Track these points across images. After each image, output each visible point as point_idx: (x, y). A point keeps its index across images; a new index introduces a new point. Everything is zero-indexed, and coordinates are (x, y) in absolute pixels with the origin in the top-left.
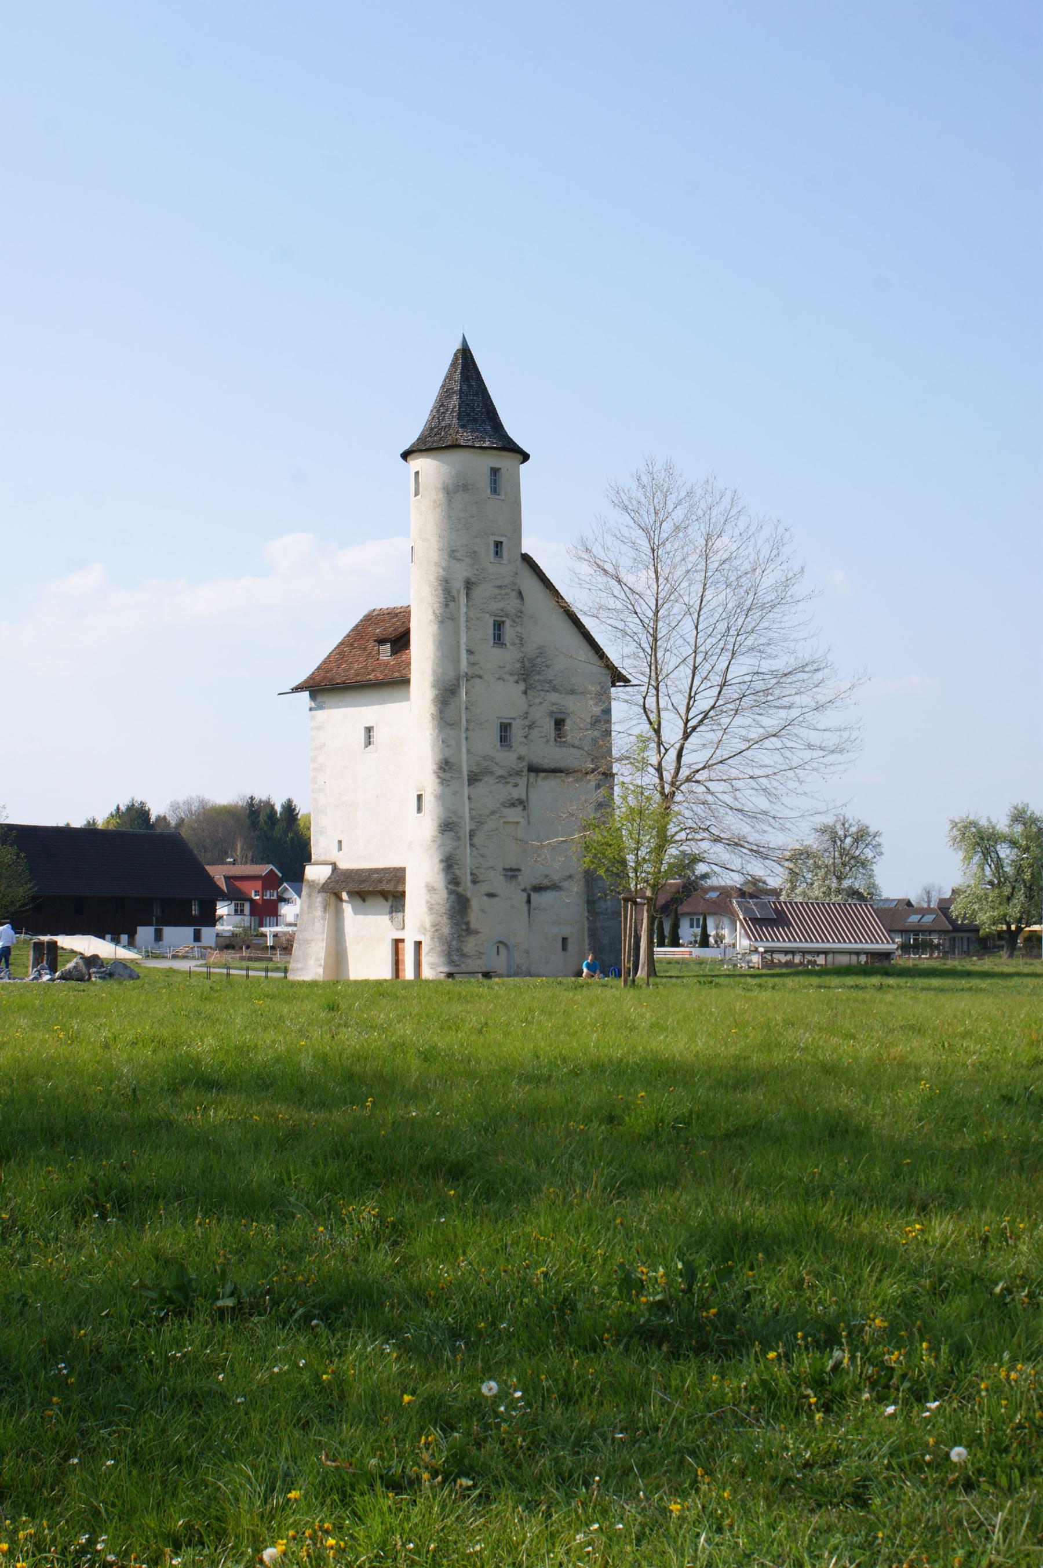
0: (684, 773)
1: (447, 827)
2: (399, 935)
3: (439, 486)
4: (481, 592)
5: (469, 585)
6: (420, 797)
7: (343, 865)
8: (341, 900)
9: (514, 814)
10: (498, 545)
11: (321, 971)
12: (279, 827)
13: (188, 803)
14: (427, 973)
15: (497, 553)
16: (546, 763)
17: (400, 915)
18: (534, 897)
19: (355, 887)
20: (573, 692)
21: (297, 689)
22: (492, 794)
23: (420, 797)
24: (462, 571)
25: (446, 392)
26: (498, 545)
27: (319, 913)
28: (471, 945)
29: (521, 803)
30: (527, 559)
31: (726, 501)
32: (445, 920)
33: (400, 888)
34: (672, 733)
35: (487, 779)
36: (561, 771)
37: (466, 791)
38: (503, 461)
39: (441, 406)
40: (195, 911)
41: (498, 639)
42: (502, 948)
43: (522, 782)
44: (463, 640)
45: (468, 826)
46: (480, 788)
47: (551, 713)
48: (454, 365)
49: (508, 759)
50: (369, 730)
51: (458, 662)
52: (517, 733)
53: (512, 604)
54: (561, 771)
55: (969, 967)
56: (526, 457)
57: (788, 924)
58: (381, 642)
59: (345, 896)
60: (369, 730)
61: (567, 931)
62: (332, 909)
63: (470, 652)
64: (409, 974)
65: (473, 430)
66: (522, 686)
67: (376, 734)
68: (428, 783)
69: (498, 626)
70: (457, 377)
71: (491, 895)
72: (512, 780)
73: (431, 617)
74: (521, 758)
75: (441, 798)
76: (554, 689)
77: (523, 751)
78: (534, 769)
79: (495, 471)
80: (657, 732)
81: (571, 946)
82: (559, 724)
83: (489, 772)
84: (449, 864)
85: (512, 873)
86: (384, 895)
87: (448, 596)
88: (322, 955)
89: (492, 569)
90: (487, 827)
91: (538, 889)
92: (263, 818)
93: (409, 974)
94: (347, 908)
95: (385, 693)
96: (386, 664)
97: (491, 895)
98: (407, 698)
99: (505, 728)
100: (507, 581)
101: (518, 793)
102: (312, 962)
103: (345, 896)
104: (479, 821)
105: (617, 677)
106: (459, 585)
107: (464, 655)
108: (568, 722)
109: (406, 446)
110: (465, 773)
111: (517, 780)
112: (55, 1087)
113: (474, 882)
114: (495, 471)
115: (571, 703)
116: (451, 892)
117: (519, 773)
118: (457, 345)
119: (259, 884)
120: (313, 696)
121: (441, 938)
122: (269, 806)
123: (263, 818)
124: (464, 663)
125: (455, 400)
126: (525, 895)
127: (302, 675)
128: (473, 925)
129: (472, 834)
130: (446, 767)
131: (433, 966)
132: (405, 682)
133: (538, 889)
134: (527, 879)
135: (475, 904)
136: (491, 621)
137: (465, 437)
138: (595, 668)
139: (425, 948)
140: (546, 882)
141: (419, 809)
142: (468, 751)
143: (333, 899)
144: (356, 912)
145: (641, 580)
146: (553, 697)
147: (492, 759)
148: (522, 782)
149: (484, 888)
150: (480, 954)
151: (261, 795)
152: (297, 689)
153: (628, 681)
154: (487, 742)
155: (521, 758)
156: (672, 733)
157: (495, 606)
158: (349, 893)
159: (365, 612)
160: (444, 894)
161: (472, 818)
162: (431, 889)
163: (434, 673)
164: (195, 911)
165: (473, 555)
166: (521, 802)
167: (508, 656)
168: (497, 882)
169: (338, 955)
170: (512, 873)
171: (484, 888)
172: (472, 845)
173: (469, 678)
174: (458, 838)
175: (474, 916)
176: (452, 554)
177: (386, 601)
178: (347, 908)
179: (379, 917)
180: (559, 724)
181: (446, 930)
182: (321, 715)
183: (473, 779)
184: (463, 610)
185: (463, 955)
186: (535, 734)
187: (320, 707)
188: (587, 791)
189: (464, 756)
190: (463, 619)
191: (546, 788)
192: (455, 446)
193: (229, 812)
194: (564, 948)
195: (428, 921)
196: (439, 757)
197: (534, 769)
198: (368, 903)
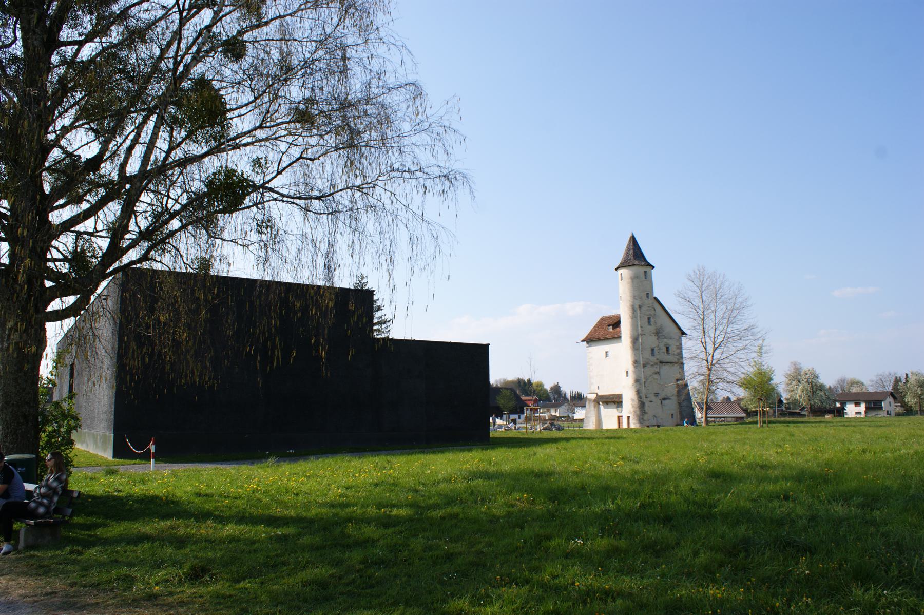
0: (714, 362)
1: (637, 381)
2: (620, 415)
3: (629, 277)
4: (644, 309)
5: (640, 307)
6: (627, 372)
7: (599, 394)
8: (599, 404)
9: (656, 376)
10: (647, 294)
11: (594, 426)
12: (527, 386)
13: (500, 380)
14: (632, 426)
15: (647, 297)
16: (664, 361)
17: (620, 409)
18: (663, 402)
19: (604, 400)
20: (671, 339)
21: (582, 341)
22: (649, 370)
23: (627, 372)
24: (637, 303)
25: (628, 249)
26: (647, 294)
27: (593, 408)
28: (646, 417)
29: (658, 373)
30: (655, 298)
31: (721, 278)
32: (638, 410)
33: (620, 400)
34: (710, 348)
35: (648, 366)
36: (671, 363)
37: (642, 370)
38: (647, 269)
39: (627, 253)
40: (519, 410)
41: (649, 323)
42: (655, 419)
43: (658, 366)
44: (639, 324)
45: (643, 380)
46: (646, 368)
47: (665, 345)
48: (630, 241)
49: (653, 359)
50: (607, 352)
51: (638, 330)
52: (656, 351)
53: (652, 312)
54: (671, 363)
55: (804, 420)
56: (653, 267)
57: (712, 409)
58: (609, 326)
59: (601, 403)
60: (607, 352)
61: (673, 412)
62: (596, 407)
63: (641, 327)
64: (625, 426)
65: (638, 260)
66: (657, 337)
67: (609, 354)
68: (631, 368)
69: (649, 319)
70: (632, 244)
71: (651, 402)
72: (655, 366)
73: (628, 316)
74: (657, 359)
75: (635, 372)
76: (665, 338)
77: (658, 357)
78: (661, 363)
79: (645, 272)
80: (706, 349)
81: (674, 416)
82: (667, 348)
83: (648, 364)
84: (638, 392)
85: (657, 395)
86: (614, 402)
87: (634, 310)
88: (594, 421)
89: (646, 302)
90: (649, 381)
91: (664, 399)
92: (522, 384)
93: (625, 426)
94: (602, 407)
95: (612, 341)
96: (611, 332)
97: (651, 402)
98: (621, 342)
99: (652, 350)
100: (651, 305)
101: (657, 370)
102: (591, 423)
103: (601, 403)
104: (646, 379)
105: (683, 333)
106: (637, 307)
107: (639, 328)
108: (670, 348)
109: (616, 267)
110: (642, 363)
111: (657, 366)
112: (713, 467)
113: (646, 398)
114: (645, 272)
115: (670, 342)
116: (639, 401)
117: (657, 364)
118: (630, 235)
119: (532, 402)
120: (588, 343)
121: (637, 415)
122: (523, 380)
123: (522, 384)
124: (640, 331)
125: (632, 251)
126: (660, 401)
127: (584, 336)
128: (646, 411)
129: (645, 383)
130: (636, 363)
131: (634, 424)
132: (620, 337)
133: (664, 399)
134: (662, 395)
135: (646, 404)
136: (647, 317)
137: (636, 262)
138: (677, 331)
139: (631, 419)
140: (666, 397)
141: (627, 376)
142: (643, 357)
143: (597, 404)
144: (605, 408)
145: (697, 302)
146: (665, 340)
147: (649, 360)
148: (658, 366)
149: (649, 399)
150: (649, 420)
151: (521, 377)
152: (582, 341)
153: (686, 334)
154: (648, 354)
155: (657, 359)
156: (710, 348)
157: (648, 313)
158: (603, 403)
159: (598, 319)
160: (637, 401)
161: (644, 378)
162: (633, 400)
163: (631, 334)
164: (519, 410)
165: (641, 297)
166: (658, 373)
167: (652, 328)
168: (653, 398)
169: (599, 421)
170: (657, 395)
171: (649, 399)
172: (645, 386)
173: (641, 335)
174: (640, 384)
175: (646, 408)
176: (634, 297)
177: (613, 312)
178: (602, 407)
179: (613, 410)
180: (667, 348)
181: (638, 413)
182: (590, 348)
183: (644, 366)
184: (639, 314)
185: (644, 420)
186: (661, 352)
187: (590, 346)
188: (676, 367)
189: (641, 359)
190: (639, 317)
191: (665, 368)
192: (634, 265)
193: (512, 382)
194: (672, 417)
195: (632, 410)
196: (633, 359)
197: (661, 363)
198: (609, 405)
